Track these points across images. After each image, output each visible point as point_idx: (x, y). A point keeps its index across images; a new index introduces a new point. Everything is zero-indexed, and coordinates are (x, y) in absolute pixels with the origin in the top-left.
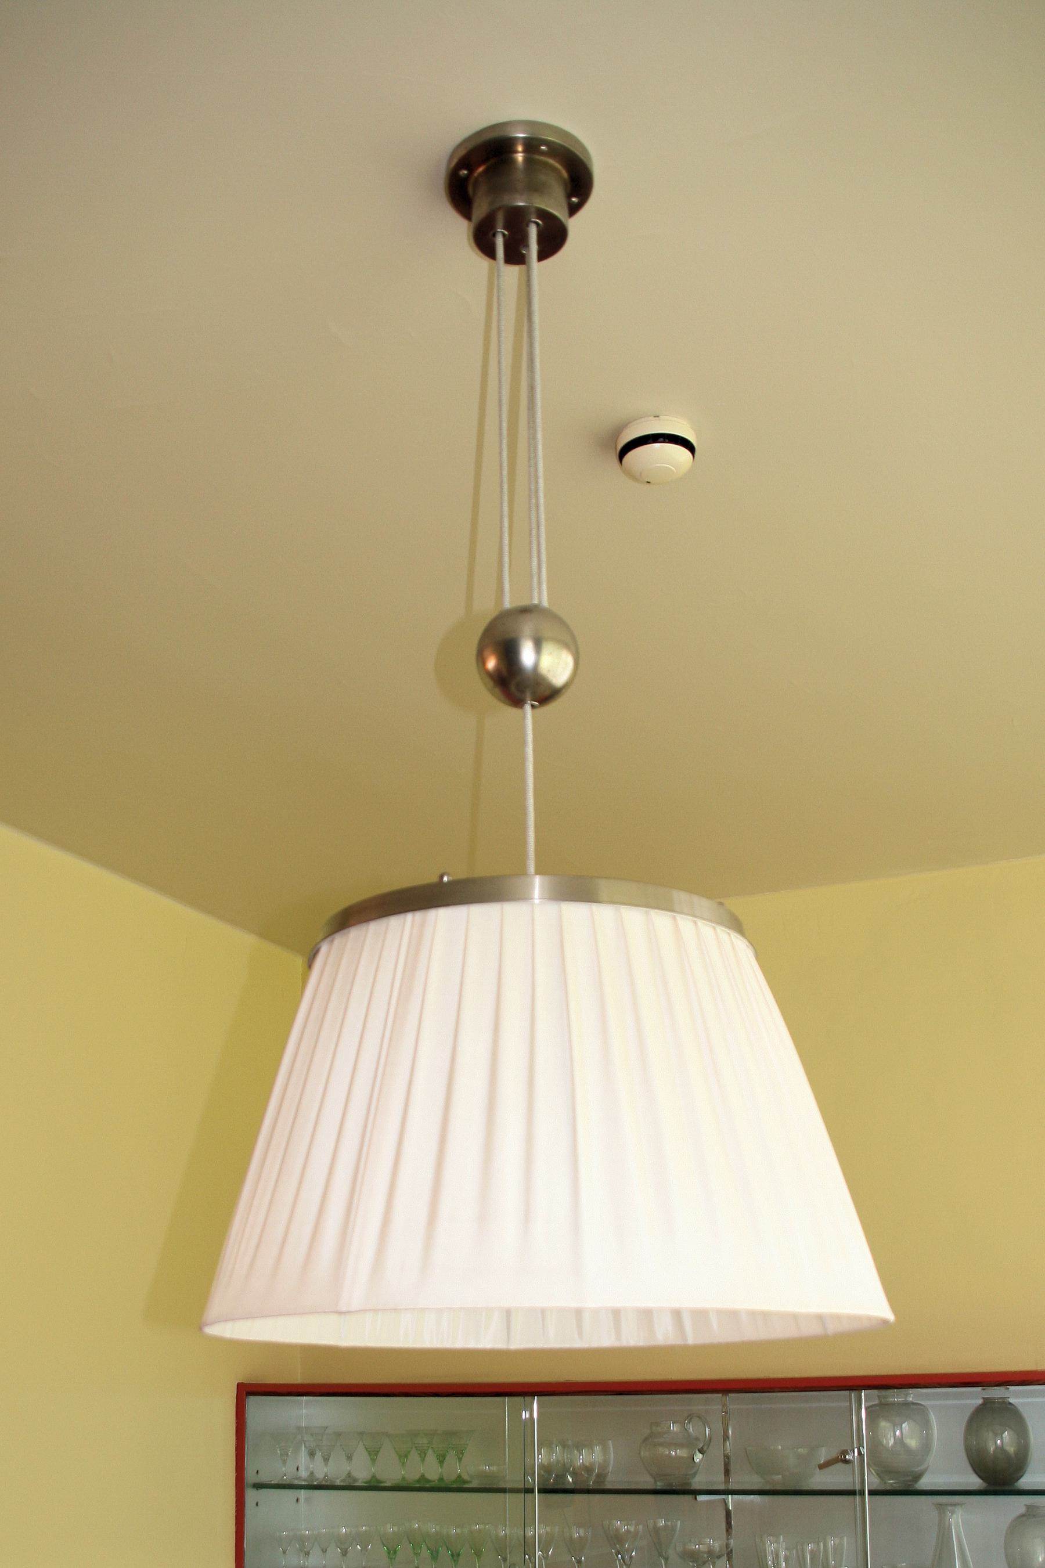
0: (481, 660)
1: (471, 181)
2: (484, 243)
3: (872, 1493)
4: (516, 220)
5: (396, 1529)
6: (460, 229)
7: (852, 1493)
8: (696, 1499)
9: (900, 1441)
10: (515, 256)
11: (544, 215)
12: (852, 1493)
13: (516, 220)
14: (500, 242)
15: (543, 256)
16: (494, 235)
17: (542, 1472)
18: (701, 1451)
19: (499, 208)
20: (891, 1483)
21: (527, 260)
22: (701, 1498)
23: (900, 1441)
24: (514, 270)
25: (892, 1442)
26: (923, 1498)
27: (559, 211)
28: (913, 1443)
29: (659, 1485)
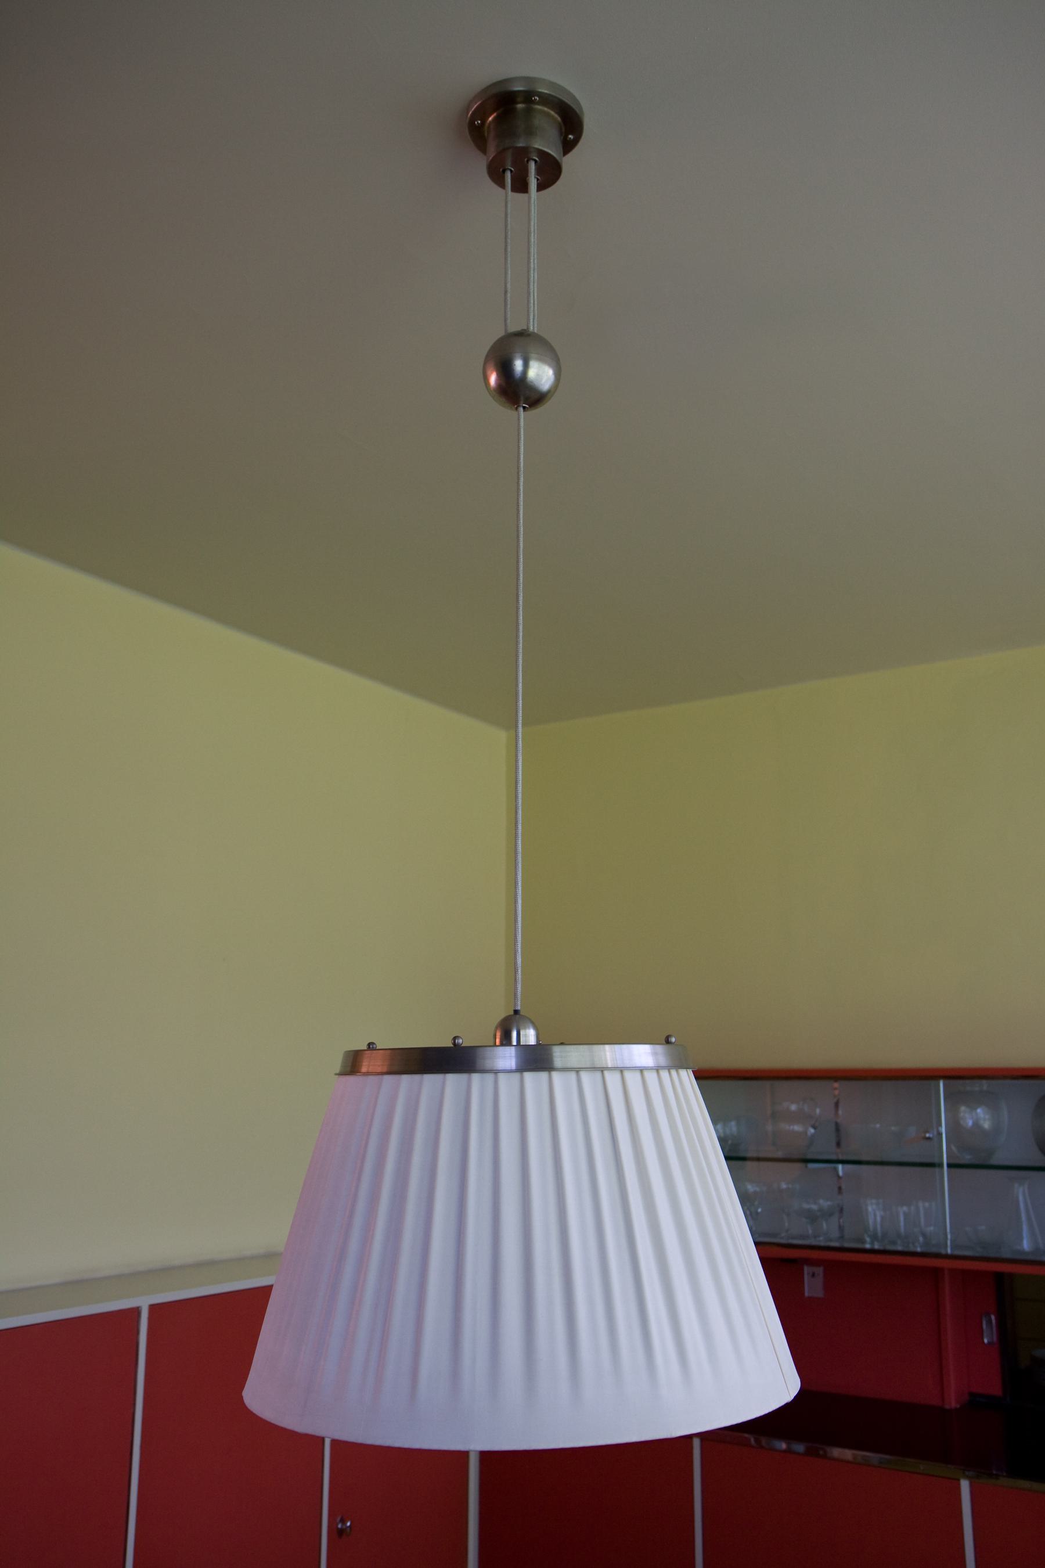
0: (486, 379)
1: (486, 128)
2: (496, 175)
3: (934, 1165)
4: (522, 156)
5: (829, 1203)
6: (480, 164)
7: (931, 1165)
8: (806, 1167)
9: (976, 1125)
10: (521, 186)
11: (542, 154)
12: (931, 1165)
13: (522, 156)
14: (508, 176)
15: (541, 187)
16: (504, 171)
17: (953, 1148)
18: (814, 1127)
19: (508, 149)
20: (967, 1158)
21: (529, 190)
22: (811, 1166)
23: (976, 1125)
24: (521, 197)
25: (970, 1123)
26: (992, 1172)
27: (553, 151)
28: (987, 1125)
29: (780, 1154)
